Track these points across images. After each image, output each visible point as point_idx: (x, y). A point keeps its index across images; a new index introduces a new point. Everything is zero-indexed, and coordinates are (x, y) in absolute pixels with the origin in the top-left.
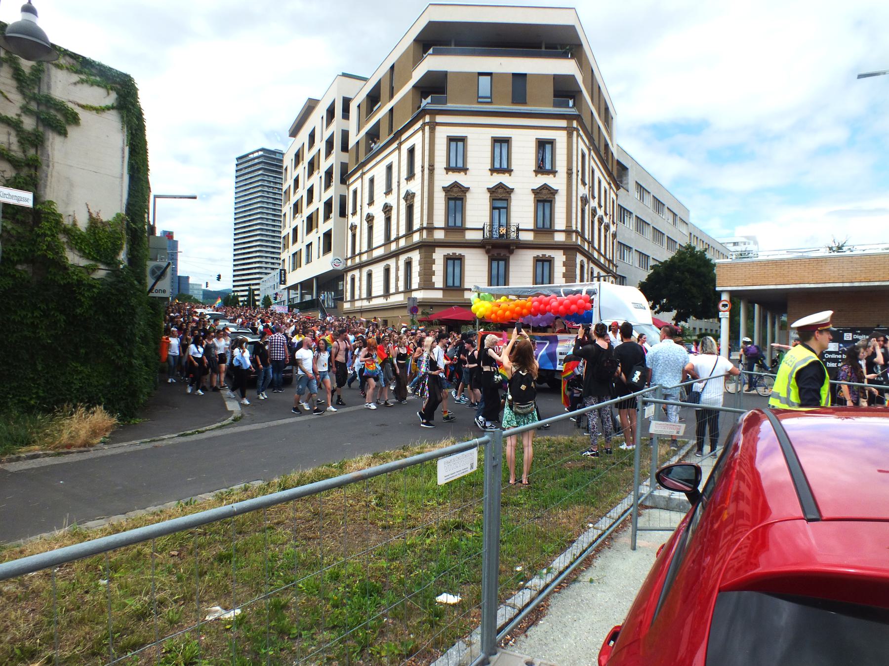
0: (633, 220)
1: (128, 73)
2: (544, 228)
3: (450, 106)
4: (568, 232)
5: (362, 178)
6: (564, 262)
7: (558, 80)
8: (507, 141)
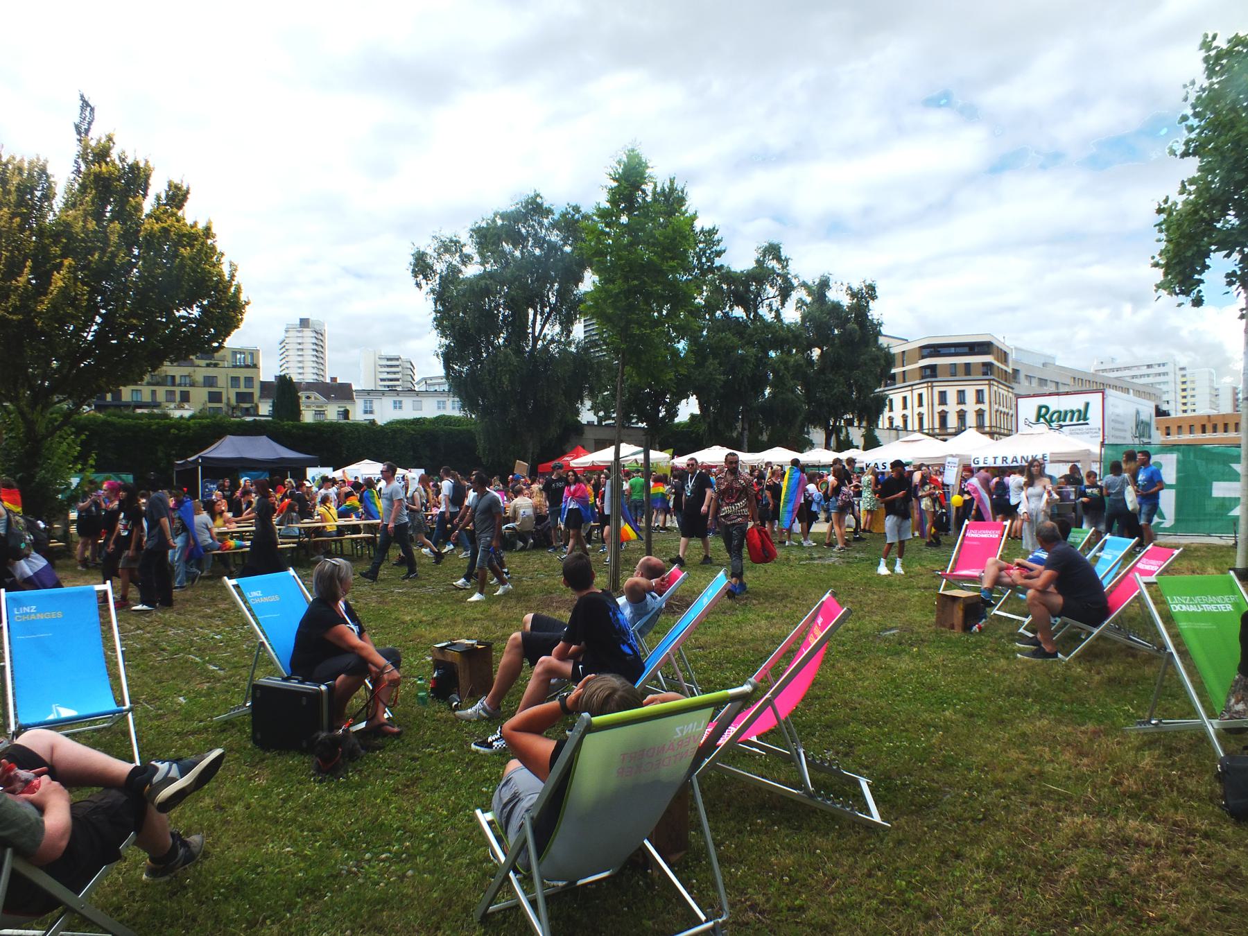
0: (1036, 380)
3: (939, 379)
4: (991, 427)
5: (1001, 166)
7: (984, 364)
8: (963, 391)
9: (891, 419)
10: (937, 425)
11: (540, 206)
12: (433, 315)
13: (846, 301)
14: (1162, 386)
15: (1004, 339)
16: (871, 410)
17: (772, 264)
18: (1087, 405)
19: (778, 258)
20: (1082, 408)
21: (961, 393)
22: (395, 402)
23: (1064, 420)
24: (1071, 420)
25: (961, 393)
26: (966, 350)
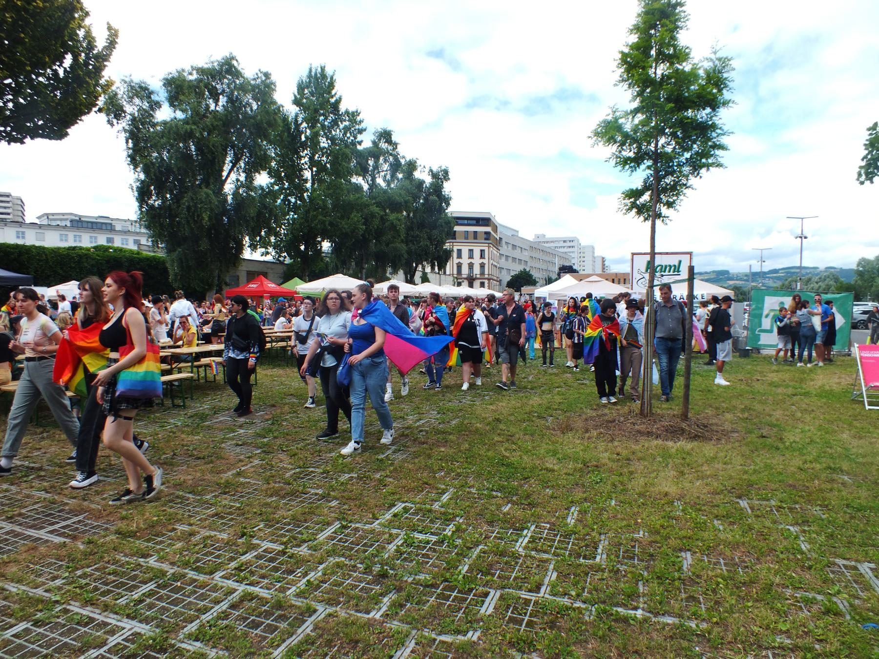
1: (63, 140)
2: (482, 273)
3: (457, 241)
4: (489, 275)
6: (834, 344)
9: (459, 266)
10: (455, 272)
11: (231, 66)
12: (125, 154)
13: (428, 180)
14: (571, 254)
15: (499, 219)
16: (441, 259)
17: (384, 145)
18: (680, 262)
19: (389, 141)
20: (677, 264)
21: (471, 251)
22: (18, 232)
23: (665, 272)
24: (669, 272)
25: (471, 251)
26: (474, 222)
